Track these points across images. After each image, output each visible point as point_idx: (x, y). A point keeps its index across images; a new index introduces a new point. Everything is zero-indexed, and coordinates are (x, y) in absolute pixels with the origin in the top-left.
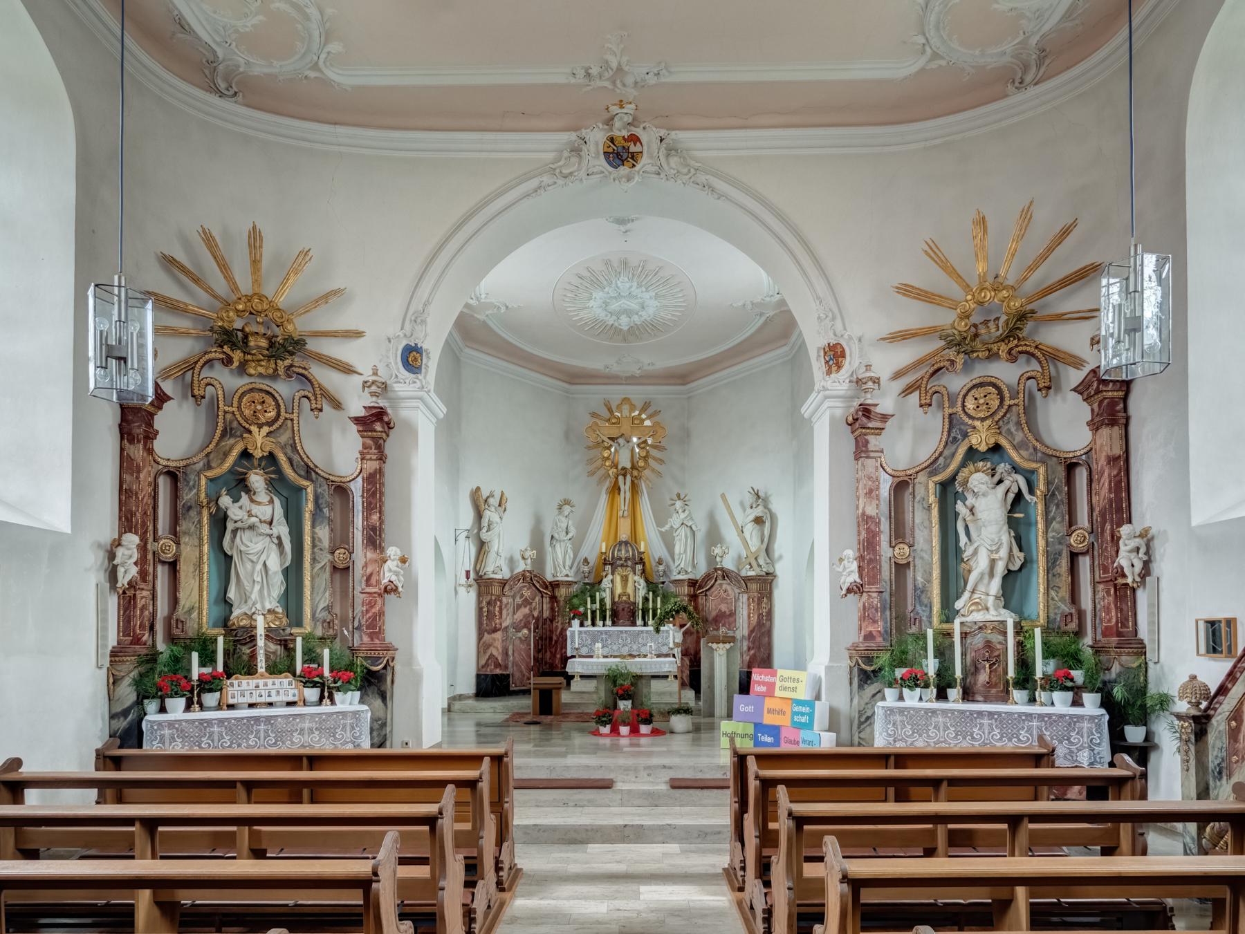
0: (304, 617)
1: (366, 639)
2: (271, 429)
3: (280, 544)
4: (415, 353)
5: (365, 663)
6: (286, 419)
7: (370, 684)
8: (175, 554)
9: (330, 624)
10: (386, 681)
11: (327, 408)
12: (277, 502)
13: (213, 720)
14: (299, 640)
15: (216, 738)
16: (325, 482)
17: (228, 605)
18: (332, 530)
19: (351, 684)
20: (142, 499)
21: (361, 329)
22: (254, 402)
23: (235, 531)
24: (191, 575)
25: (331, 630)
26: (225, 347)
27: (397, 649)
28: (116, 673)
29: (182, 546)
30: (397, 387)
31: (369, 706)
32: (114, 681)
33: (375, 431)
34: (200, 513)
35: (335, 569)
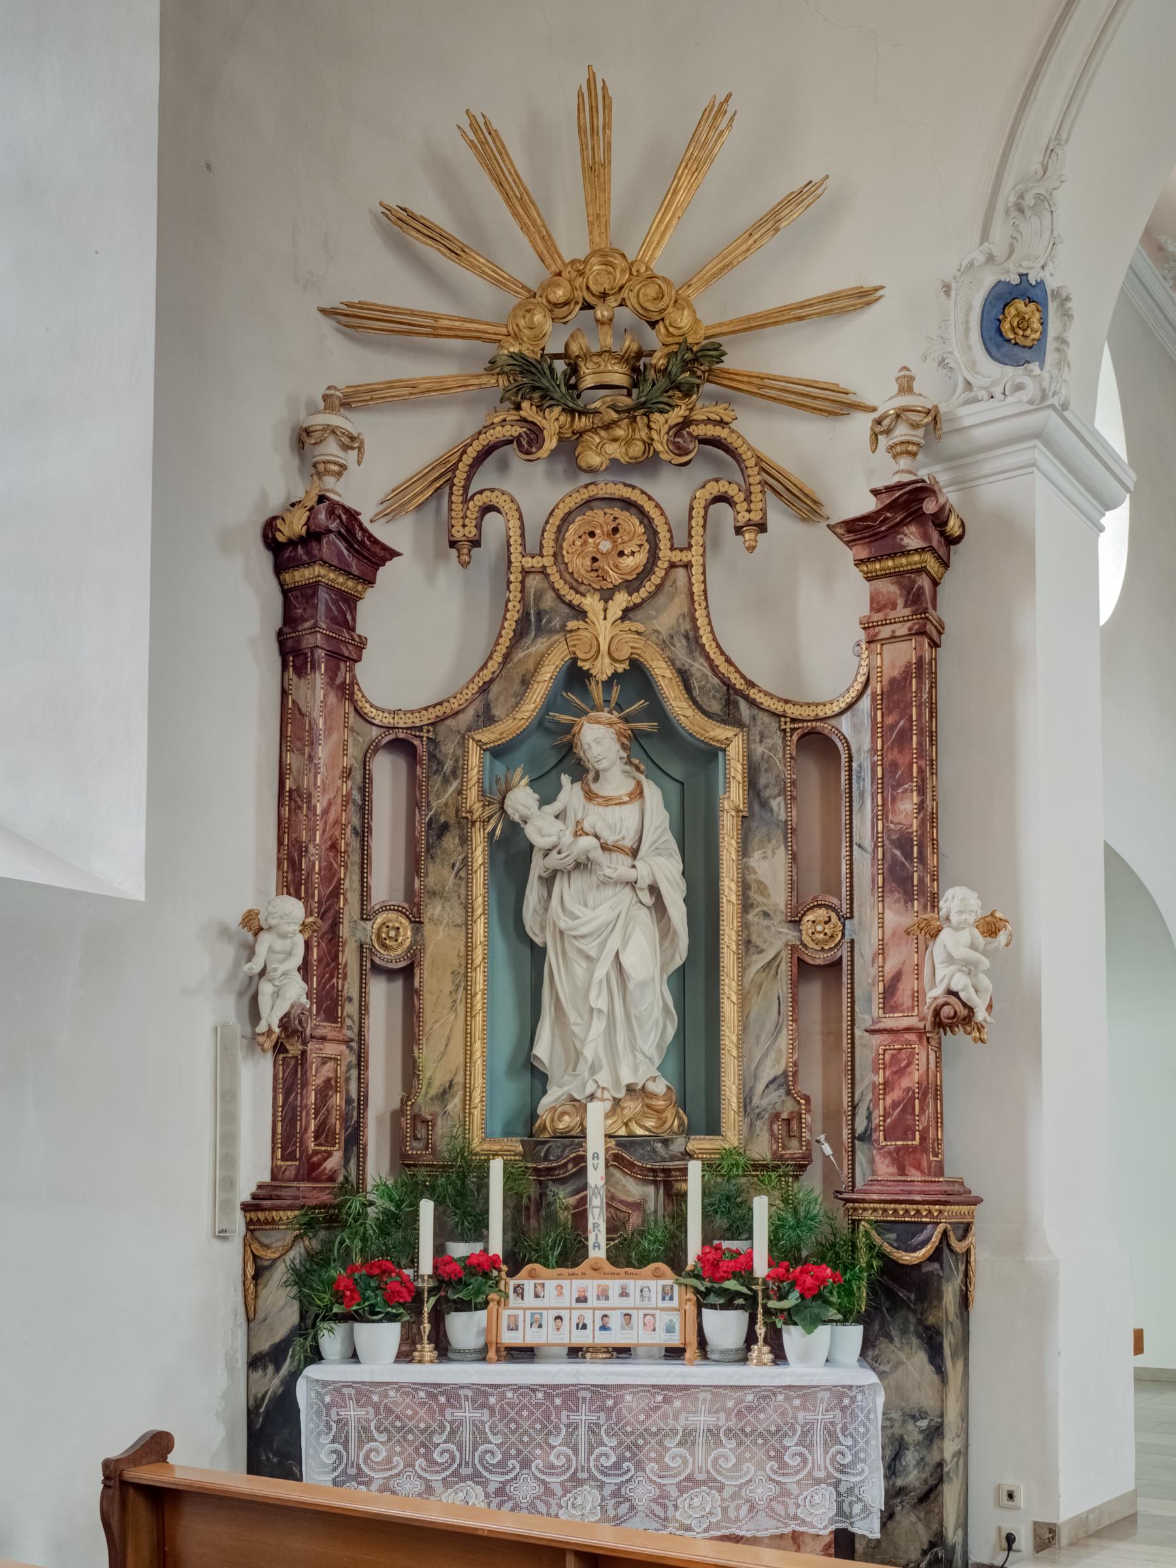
0: (724, 1105)
1: (885, 1169)
2: (636, 598)
3: (659, 907)
4: (1020, 304)
5: (878, 1240)
6: (673, 565)
7: (896, 1304)
8: (410, 948)
9: (790, 1125)
10: (940, 1297)
11: (779, 519)
12: (653, 793)
13: (463, 1387)
14: (695, 1169)
15: (467, 1438)
16: (775, 725)
17: (538, 1078)
18: (794, 857)
19: (827, 1302)
20: (326, 812)
21: (869, 284)
22: (592, 534)
23: (549, 881)
24: (448, 1002)
25: (794, 1143)
26: (525, 405)
27: (977, 1201)
28: (260, 1252)
29: (428, 928)
30: (968, 415)
31: (881, 1375)
32: (258, 1271)
33: (906, 553)
34: (465, 840)
35: (803, 969)
